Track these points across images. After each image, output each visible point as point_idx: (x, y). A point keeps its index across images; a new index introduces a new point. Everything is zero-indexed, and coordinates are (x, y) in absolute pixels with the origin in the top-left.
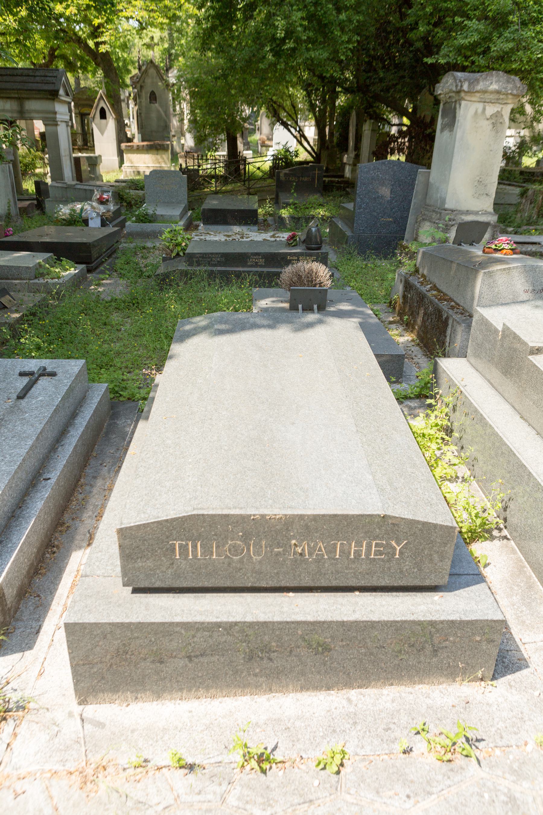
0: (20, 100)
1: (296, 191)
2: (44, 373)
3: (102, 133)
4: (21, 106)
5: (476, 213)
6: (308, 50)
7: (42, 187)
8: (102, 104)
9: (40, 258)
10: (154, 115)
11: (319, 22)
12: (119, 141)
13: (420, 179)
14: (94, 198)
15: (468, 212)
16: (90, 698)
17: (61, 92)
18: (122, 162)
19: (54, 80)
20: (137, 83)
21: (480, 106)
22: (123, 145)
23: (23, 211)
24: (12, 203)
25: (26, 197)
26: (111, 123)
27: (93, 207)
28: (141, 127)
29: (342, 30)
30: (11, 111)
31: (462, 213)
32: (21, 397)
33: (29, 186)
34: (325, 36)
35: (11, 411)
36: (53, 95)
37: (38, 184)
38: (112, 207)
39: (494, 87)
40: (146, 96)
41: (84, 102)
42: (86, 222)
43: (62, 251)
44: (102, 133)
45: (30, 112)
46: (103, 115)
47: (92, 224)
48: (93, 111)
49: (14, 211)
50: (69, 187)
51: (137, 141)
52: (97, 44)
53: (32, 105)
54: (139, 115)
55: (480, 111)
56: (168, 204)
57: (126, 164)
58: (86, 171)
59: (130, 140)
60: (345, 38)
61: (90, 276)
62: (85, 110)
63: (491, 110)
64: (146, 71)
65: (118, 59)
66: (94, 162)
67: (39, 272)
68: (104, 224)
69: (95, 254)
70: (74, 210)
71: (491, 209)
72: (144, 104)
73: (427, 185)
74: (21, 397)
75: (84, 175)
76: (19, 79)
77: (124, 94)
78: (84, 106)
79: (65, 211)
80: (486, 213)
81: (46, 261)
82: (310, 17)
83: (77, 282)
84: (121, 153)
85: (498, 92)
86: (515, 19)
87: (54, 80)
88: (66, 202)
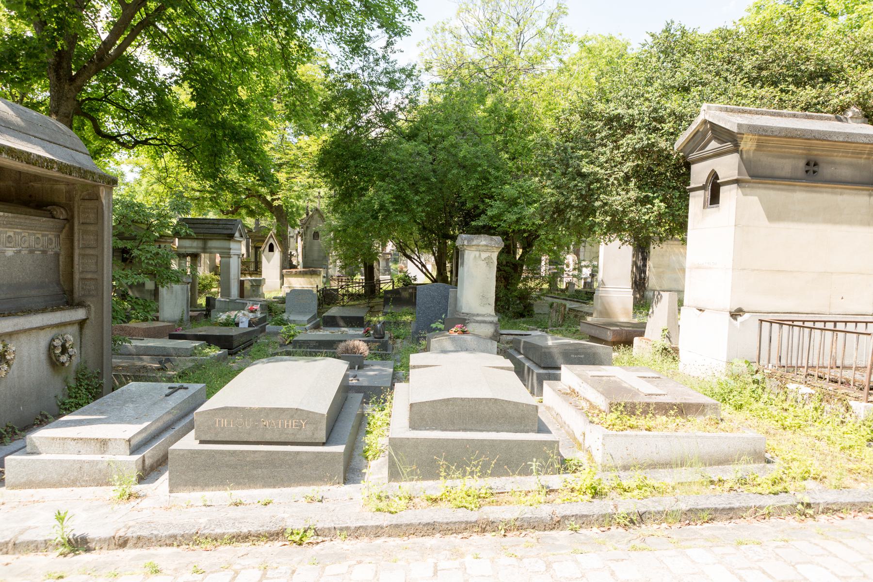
0: (205, 240)
1: (393, 304)
2: (181, 388)
3: (269, 261)
4: (205, 244)
5: (483, 316)
6: (396, 216)
7: (212, 301)
8: (271, 241)
9: (197, 344)
10: (316, 248)
11: (404, 199)
12: (283, 267)
13: (451, 295)
14: (246, 308)
15: (478, 315)
16: (175, 489)
17: (237, 234)
18: (282, 284)
19: (232, 227)
20: (306, 225)
21: (477, 253)
22: (284, 271)
23: (192, 319)
24: (185, 312)
25: (199, 309)
26: (277, 254)
27: (244, 315)
28: (305, 256)
29: (419, 205)
30: (196, 248)
31: (474, 315)
32: (167, 396)
33: (202, 301)
34: (407, 207)
35: (161, 400)
36: (231, 237)
37: (208, 299)
38: (259, 315)
39: (483, 243)
40: (309, 237)
41: (257, 240)
42: (237, 325)
43: (210, 340)
44: (269, 261)
45: (210, 248)
46: (271, 249)
47: (241, 325)
48: (264, 246)
49: (185, 317)
50: (233, 301)
51: (300, 268)
52: (273, 200)
53: (212, 244)
54: (304, 248)
55: (477, 255)
56: (300, 313)
57: (285, 285)
58: (249, 291)
59: (295, 267)
60: (420, 209)
61: (229, 357)
62: (258, 245)
63: (484, 255)
64: (312, 216)
65: (292, 207)
66: (258, 285)
67: (192, 353)
68: (250, 325)
69: (235, 344)
70: (229, 316)
71: (493, 313)
72: (308, 240)
73: (456, 299)
74: (167, 396)
75: (246, 293)
76: (207, 226)
77: (291, 232)
78: (259, 241)
79: (223, 317)
80: (490, 315)
81: (201, 346)
82: (397, 197)
83: (218, 358)
84: (282, 277)
85: (487, 246)
86: (522, 201)
87: (232, 227)
88: (224, 312)
